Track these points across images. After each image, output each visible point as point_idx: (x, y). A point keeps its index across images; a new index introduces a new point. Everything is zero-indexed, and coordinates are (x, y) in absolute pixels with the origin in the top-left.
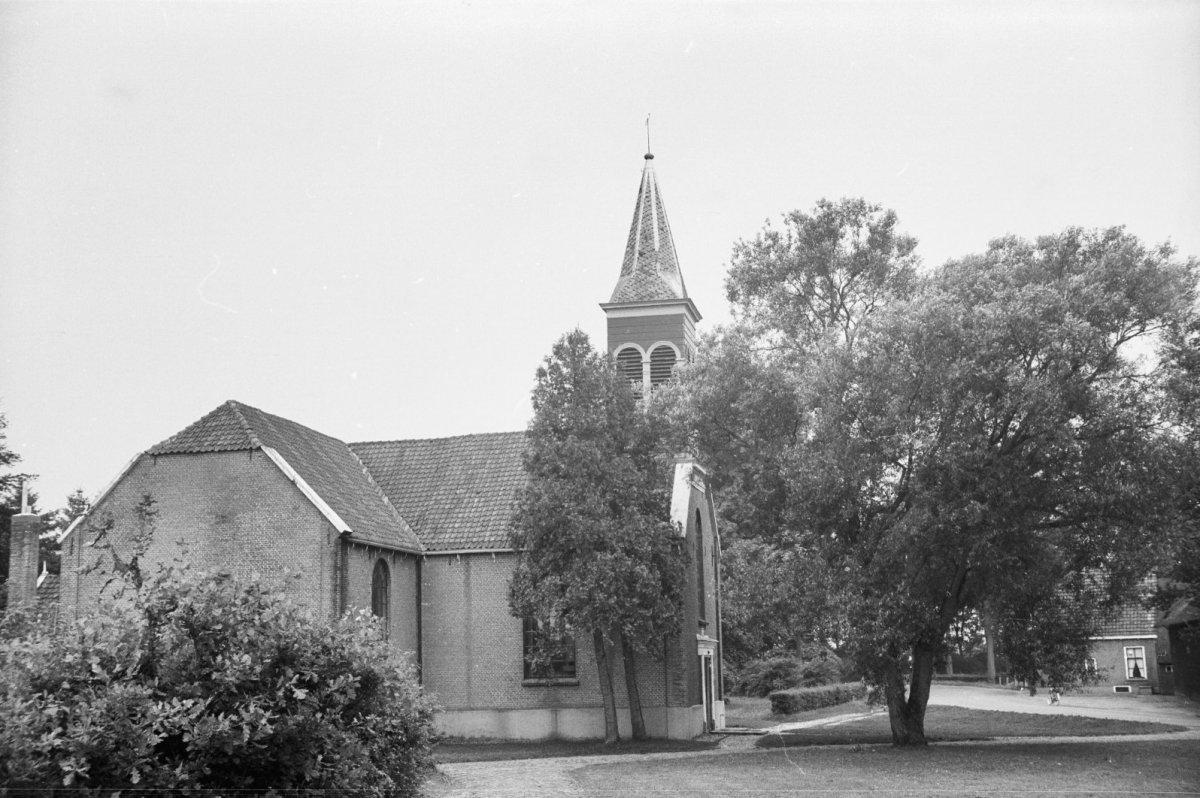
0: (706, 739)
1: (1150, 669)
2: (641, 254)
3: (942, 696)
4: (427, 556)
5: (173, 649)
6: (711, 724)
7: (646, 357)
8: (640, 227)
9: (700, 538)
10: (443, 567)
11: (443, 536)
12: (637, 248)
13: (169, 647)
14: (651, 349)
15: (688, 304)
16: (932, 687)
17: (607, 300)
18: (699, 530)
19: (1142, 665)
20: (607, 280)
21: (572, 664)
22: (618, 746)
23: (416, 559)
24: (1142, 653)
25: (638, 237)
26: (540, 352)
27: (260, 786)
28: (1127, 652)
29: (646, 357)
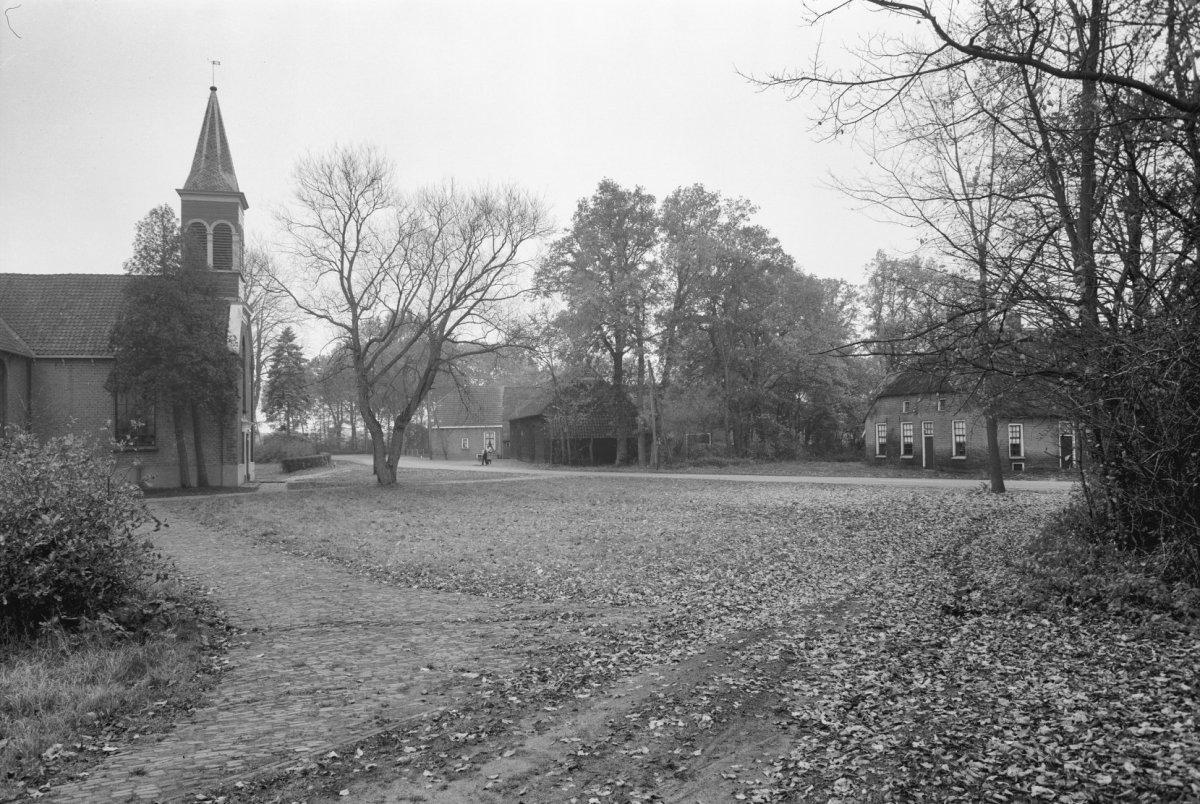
0: (246, 486)
1: (497, 445)
2: (207, 158)
3: (405, 463)
4: (37, 359)
5: (984, 269)
6: (248, 477)
7: (210, 230)
8: (206, 138)
9: (244, 356)
10: (51, 369)
11: (49, 345)
12: (204, 152)
13: (975, 274)
14: (215, 224)
15: (241, 196)
16: (401, 458)
17: (181, 187)
18: (244, 349)
19: (493, 442)
20: (181, 175)
21: (153, 437)
22: (184, 488)
23: (28, 362)
24: (494, 435)
25: (205, 145)
26: (142, 214)
27: (1170, 800)
28: (486, 435)
29: (210, 230)
